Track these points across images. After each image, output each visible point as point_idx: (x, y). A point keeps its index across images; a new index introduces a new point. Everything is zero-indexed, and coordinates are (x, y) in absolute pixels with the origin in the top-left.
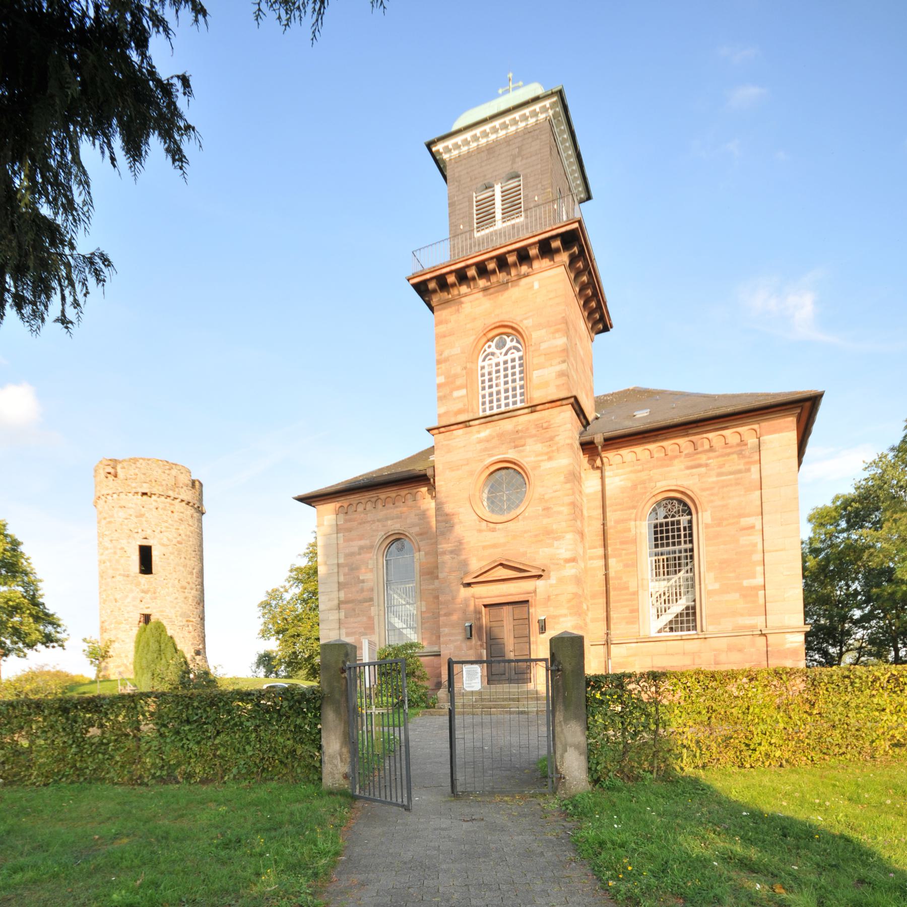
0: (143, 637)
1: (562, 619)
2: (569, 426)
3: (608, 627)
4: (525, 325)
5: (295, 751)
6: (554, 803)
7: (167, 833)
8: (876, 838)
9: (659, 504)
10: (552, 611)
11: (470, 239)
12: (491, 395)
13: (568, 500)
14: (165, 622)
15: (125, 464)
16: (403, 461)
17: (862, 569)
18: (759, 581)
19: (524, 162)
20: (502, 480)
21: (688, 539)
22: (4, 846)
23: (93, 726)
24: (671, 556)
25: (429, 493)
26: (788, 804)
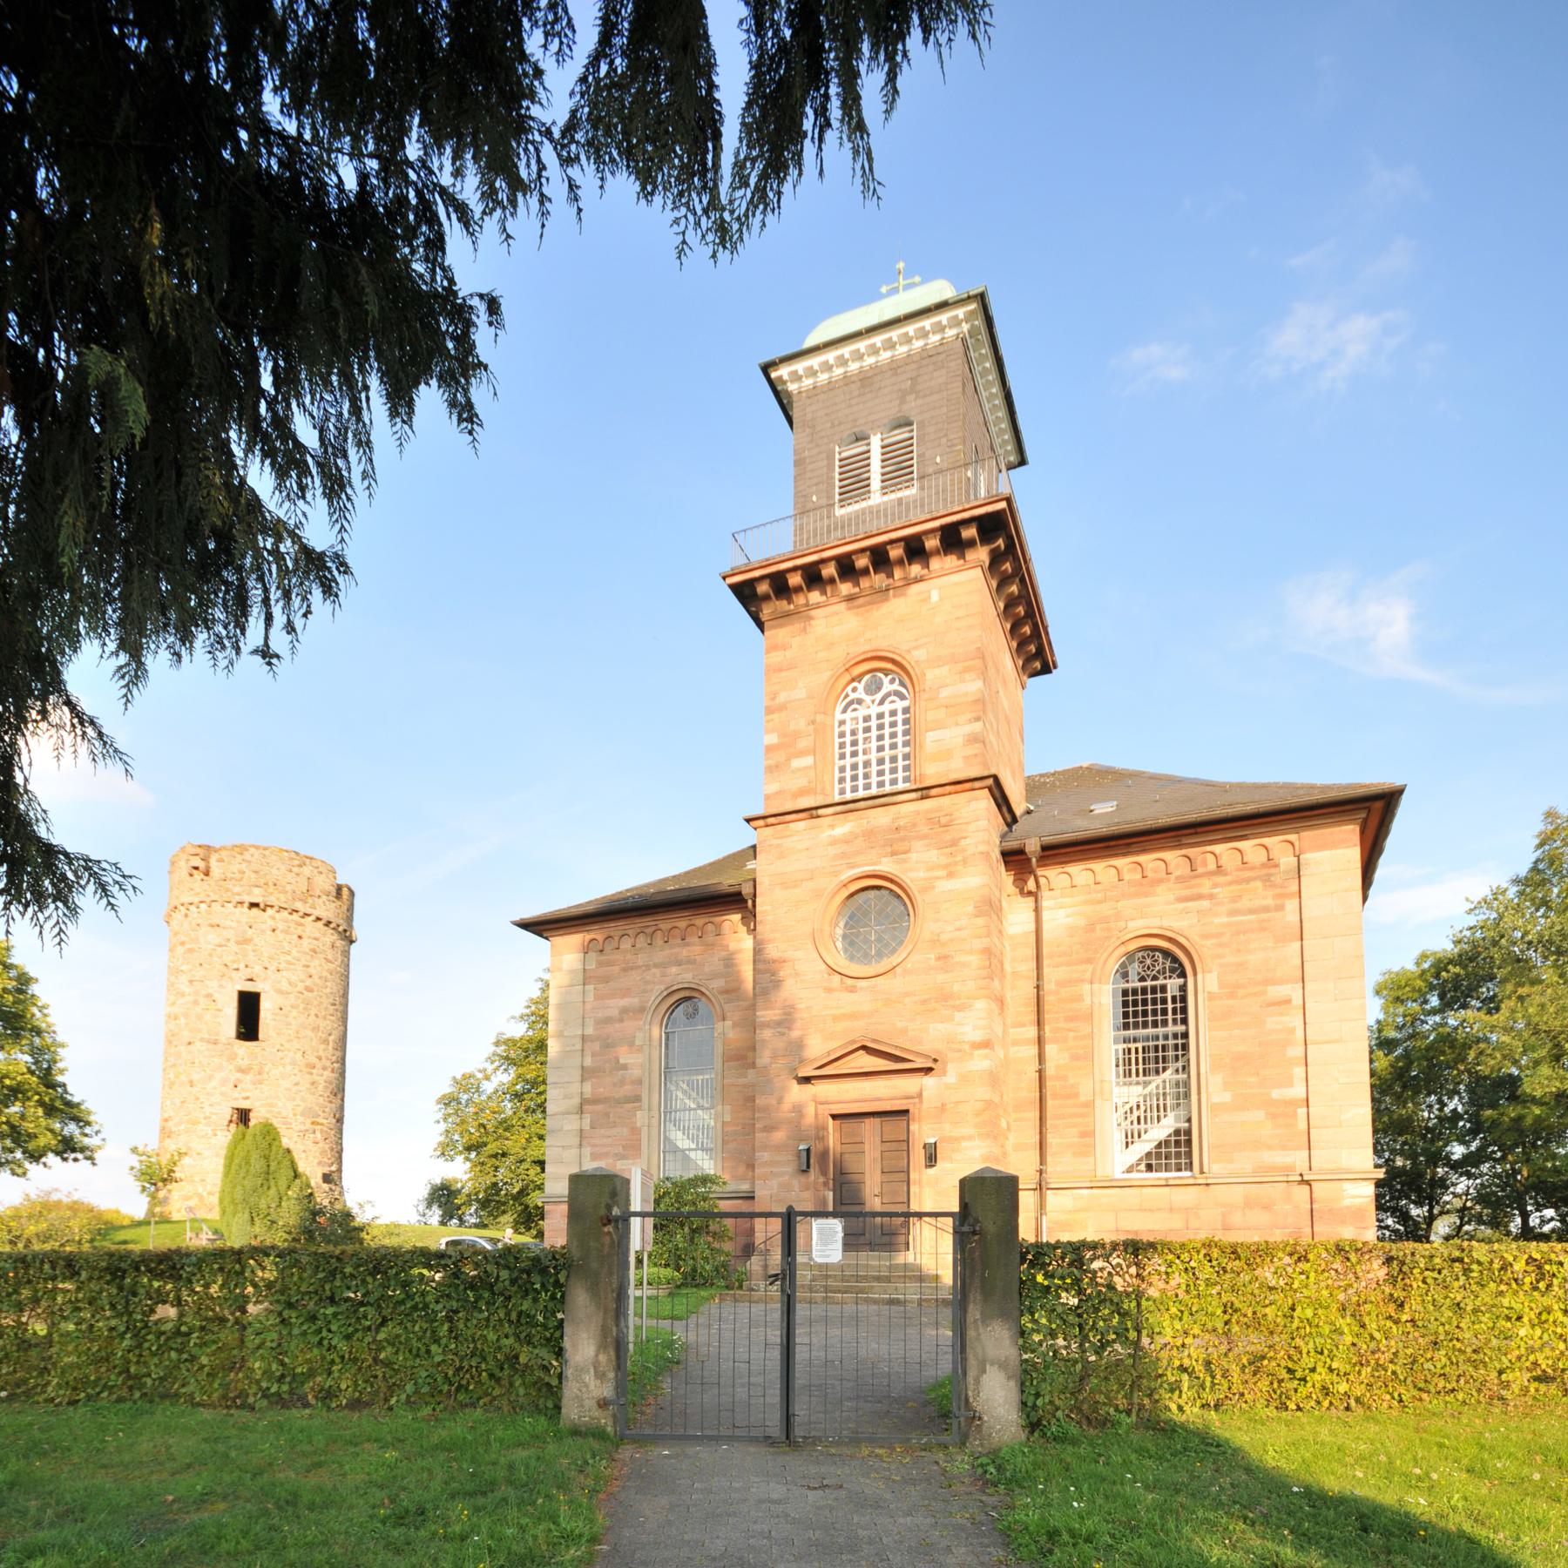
0: (239, 1148)
1: (964, 1144)
2: (983, 823)
3: (1042, 1161)
4: (915, 657)
5: (517, 1357)
6: (963, 1461)
7: (295, 1495)
8: (1518, 1539)
9: (1130, 956)
10: (948, 1129)
11: (828, 517)
12: (854, 767)
13: (978, 944)
14: (276, 1122)
15: (224, 854)
16: (695, 870)
17: (1465, 1077)
18: (1298, 1091)
19: (920, 402)
20: (870, 906)
21: (1179, 1016)
22: (4, 1509)
23: (164, 1302)
24: (1151, 1044)
25: (744, 924)
26: (1366, 1474)
